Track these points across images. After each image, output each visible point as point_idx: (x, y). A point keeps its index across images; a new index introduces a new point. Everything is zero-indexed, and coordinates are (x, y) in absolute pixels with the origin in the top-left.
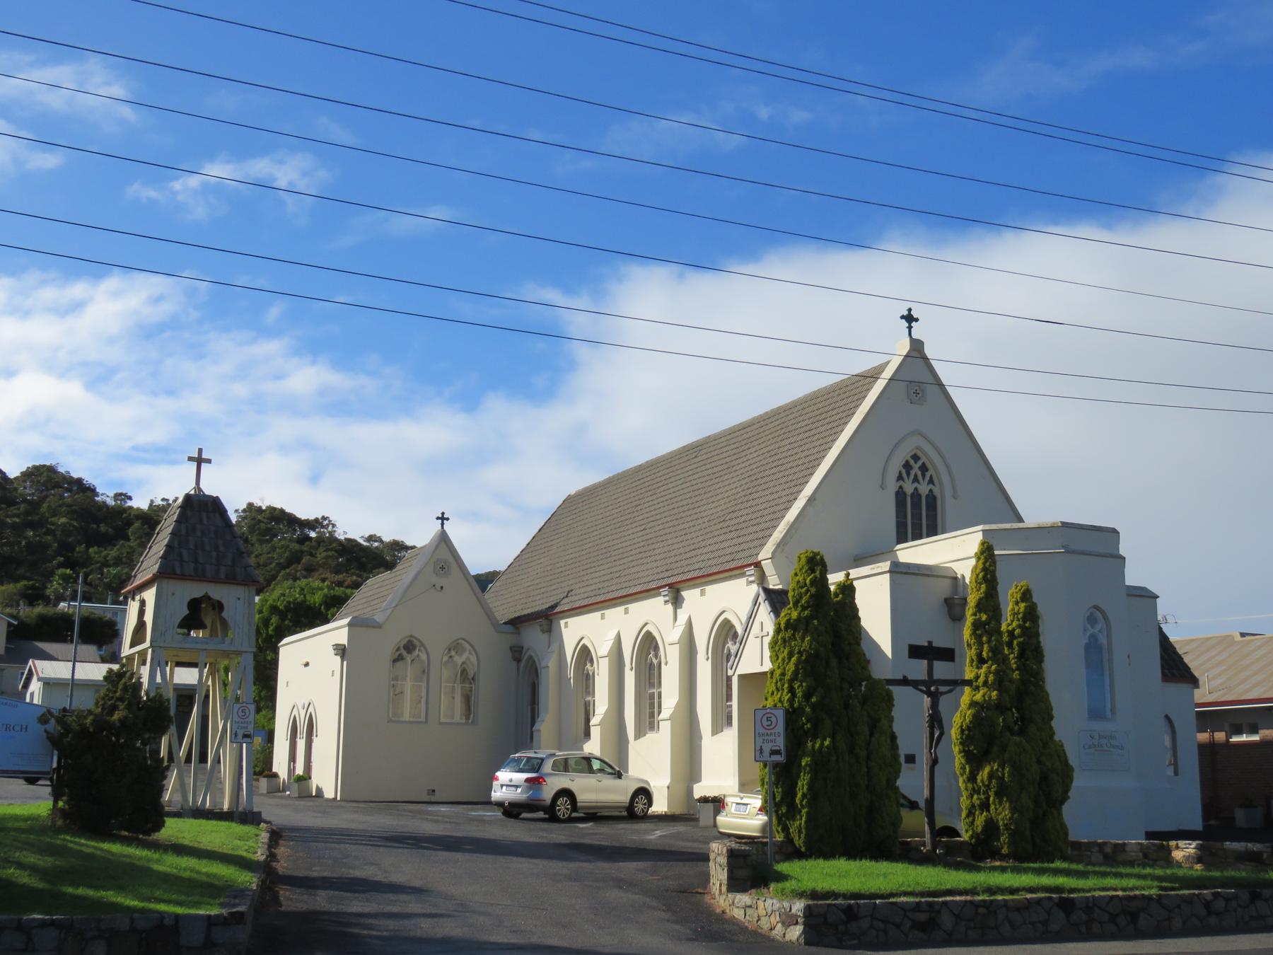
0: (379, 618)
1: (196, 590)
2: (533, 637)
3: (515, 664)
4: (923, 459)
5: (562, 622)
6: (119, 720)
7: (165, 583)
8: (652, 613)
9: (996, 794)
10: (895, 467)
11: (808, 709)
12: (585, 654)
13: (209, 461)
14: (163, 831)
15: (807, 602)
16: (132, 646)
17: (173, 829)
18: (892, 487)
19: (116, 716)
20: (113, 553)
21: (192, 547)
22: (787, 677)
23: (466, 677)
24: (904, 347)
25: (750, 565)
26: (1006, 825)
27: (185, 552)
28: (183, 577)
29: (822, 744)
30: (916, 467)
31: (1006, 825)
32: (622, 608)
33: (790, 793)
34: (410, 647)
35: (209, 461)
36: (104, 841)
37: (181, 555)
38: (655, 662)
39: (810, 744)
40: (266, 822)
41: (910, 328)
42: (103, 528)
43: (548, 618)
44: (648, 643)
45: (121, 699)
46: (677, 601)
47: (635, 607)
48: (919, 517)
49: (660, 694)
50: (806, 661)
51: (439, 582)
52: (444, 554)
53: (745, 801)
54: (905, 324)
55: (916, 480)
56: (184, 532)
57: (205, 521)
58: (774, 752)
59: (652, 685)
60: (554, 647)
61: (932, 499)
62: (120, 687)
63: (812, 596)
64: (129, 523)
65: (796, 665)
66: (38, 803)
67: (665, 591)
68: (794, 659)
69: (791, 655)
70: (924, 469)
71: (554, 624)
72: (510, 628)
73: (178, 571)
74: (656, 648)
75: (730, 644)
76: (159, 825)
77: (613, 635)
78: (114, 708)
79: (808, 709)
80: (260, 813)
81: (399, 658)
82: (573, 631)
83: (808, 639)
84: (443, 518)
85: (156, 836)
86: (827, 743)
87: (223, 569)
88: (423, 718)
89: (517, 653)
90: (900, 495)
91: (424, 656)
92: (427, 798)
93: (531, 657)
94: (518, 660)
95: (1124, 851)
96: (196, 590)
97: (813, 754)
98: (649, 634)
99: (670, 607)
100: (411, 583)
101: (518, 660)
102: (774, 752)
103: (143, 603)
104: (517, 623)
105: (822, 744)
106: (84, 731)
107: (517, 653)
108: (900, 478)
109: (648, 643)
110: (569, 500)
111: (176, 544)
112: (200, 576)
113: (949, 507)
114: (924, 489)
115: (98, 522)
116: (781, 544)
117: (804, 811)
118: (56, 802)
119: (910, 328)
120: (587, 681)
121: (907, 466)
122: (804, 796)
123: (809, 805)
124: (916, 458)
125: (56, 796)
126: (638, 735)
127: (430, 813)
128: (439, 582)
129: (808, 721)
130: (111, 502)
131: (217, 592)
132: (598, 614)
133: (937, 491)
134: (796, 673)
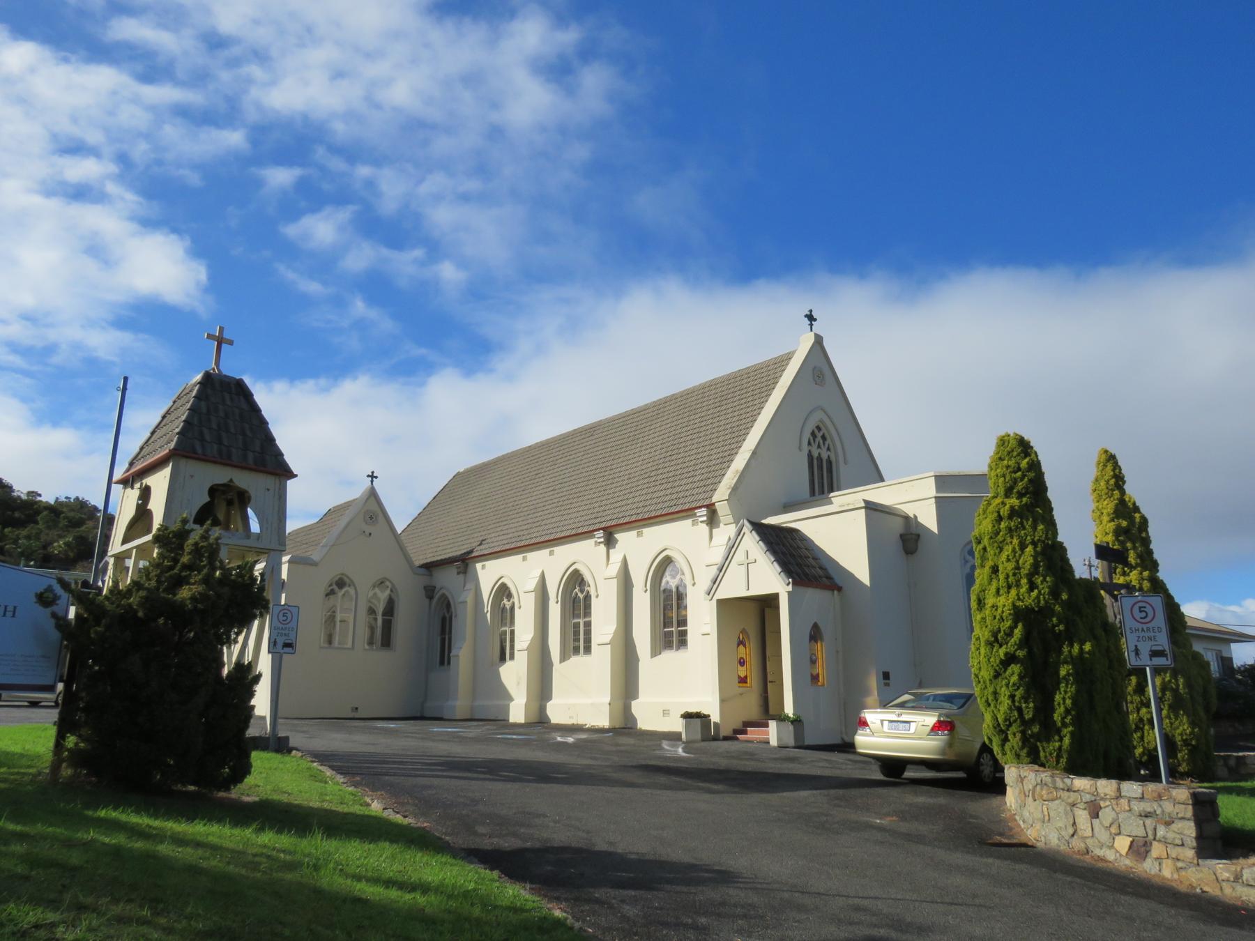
0: (316, 556)
1: (220, 475)
2: (447, 580)
3: (427, 601)
4: (824, 430)
5: (479, 566)
6: (193, 599)
7: (183, 462)
8: (586, 555)
9: (1170, 707)
10: (807, 436)
11: (1058, 608)
12: (503, 591)
13: (231, 343)
14: (249, 780)
15: (1026, 488)
16: (124, 542)
17: (268, 777)
18: (806, 448)
19: (185, 593)
20: (24, 532)
21: (214, 426)
22: (1024, 572)
23: (372, 611)
24: (807, 341)
25: (700, 507)
26: (1184, 741)
27: (206, 431)
28: (204, 459)
29: (1081, 649)
30: (819, 435)
31: (1184, 741)
32: (521, 556)
33: (1044, 709)
34: (341, 583)
35: (231, 343)
36: (191, 818)
37: (201, 433)
38: (581, 596)
39: (1066, 649)
40: (297, 750)
41: (811, 325)
42: (17, 514)
43: (464, 563)
44: (575, 580)
45: (189, 567)
46: (610, 542)
47: (559, 550)
48: (822, 480)
49: (512, 632)
50: (1043, 553)
51: (368, 529)
52: (373, 506)
53: (905, 718)
54: (807, 321)
55: (819, 447)
56: (204, 411)
57: (229, 403)
58: (1155, 654)
59: (503, 623)
60: (470, 586)
61: (829, 462)
62: (187, 548)
63: (1030, 481)
64: (38, 512)
65: (1035, 557)
66: (25, 735)
67: (600, 534)
68: (1029, 549)
69: (1023, 546)
70: (824, 438)
71: (470, 566)
72: (423, 571)
73: (199, 450)
74: (510, 596)
75: (505, 601)
76: (242, 770)
77: (538, 574)
78: (179, 582)
79: (1058, 608)
80: (287, 739)
81: (331, 593)
82: (488, 574)
83: (1041, 527)
84: (372, 476)
85: (235, 793)
86: (1087, 647)
87: (250, 456)
88: (349, 645)
89: (430, 592)
90: (810, 456)
91: (352, 591)
92: (351, 715)
93: (443, 595)
94: (430, 597)
95: (1245, 764)
96: (220, 475)
97: (1072, 660)
98: (576, 572)
99: (603, 548)
100: (346, 527)
101: (430, 597)
102: (1155, 654)
103: (146, 493)
104: (429, 567)
105: (1081, 649)
106: (127, 619)
107: (430, 592)
108: (809, 443)
109: (575, 580)
110: (458, 475)
111: (196, 421)
112: (224, 460)
113: (843, 471)
114: (825, 456)
115: (13, 510)
116: (735, 489)
117: (1065, 731)
118: (61, 737)
119: (811, 325)
120: (505, 615)
121: (813, 434)
122: (1067, 711)
123: (1077, 721)
124: (819, 428)
125: (65, 726)
126: (564, 658)
127: (377, 728)
128: (368, 529)
129: (1060, 622)
130: (24, 497)
131: (243, 480)
132: (520, 557)
133: (833, 458)
134: (1035, 566)
